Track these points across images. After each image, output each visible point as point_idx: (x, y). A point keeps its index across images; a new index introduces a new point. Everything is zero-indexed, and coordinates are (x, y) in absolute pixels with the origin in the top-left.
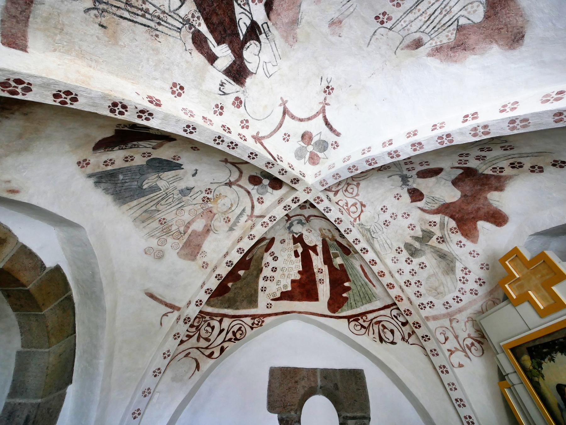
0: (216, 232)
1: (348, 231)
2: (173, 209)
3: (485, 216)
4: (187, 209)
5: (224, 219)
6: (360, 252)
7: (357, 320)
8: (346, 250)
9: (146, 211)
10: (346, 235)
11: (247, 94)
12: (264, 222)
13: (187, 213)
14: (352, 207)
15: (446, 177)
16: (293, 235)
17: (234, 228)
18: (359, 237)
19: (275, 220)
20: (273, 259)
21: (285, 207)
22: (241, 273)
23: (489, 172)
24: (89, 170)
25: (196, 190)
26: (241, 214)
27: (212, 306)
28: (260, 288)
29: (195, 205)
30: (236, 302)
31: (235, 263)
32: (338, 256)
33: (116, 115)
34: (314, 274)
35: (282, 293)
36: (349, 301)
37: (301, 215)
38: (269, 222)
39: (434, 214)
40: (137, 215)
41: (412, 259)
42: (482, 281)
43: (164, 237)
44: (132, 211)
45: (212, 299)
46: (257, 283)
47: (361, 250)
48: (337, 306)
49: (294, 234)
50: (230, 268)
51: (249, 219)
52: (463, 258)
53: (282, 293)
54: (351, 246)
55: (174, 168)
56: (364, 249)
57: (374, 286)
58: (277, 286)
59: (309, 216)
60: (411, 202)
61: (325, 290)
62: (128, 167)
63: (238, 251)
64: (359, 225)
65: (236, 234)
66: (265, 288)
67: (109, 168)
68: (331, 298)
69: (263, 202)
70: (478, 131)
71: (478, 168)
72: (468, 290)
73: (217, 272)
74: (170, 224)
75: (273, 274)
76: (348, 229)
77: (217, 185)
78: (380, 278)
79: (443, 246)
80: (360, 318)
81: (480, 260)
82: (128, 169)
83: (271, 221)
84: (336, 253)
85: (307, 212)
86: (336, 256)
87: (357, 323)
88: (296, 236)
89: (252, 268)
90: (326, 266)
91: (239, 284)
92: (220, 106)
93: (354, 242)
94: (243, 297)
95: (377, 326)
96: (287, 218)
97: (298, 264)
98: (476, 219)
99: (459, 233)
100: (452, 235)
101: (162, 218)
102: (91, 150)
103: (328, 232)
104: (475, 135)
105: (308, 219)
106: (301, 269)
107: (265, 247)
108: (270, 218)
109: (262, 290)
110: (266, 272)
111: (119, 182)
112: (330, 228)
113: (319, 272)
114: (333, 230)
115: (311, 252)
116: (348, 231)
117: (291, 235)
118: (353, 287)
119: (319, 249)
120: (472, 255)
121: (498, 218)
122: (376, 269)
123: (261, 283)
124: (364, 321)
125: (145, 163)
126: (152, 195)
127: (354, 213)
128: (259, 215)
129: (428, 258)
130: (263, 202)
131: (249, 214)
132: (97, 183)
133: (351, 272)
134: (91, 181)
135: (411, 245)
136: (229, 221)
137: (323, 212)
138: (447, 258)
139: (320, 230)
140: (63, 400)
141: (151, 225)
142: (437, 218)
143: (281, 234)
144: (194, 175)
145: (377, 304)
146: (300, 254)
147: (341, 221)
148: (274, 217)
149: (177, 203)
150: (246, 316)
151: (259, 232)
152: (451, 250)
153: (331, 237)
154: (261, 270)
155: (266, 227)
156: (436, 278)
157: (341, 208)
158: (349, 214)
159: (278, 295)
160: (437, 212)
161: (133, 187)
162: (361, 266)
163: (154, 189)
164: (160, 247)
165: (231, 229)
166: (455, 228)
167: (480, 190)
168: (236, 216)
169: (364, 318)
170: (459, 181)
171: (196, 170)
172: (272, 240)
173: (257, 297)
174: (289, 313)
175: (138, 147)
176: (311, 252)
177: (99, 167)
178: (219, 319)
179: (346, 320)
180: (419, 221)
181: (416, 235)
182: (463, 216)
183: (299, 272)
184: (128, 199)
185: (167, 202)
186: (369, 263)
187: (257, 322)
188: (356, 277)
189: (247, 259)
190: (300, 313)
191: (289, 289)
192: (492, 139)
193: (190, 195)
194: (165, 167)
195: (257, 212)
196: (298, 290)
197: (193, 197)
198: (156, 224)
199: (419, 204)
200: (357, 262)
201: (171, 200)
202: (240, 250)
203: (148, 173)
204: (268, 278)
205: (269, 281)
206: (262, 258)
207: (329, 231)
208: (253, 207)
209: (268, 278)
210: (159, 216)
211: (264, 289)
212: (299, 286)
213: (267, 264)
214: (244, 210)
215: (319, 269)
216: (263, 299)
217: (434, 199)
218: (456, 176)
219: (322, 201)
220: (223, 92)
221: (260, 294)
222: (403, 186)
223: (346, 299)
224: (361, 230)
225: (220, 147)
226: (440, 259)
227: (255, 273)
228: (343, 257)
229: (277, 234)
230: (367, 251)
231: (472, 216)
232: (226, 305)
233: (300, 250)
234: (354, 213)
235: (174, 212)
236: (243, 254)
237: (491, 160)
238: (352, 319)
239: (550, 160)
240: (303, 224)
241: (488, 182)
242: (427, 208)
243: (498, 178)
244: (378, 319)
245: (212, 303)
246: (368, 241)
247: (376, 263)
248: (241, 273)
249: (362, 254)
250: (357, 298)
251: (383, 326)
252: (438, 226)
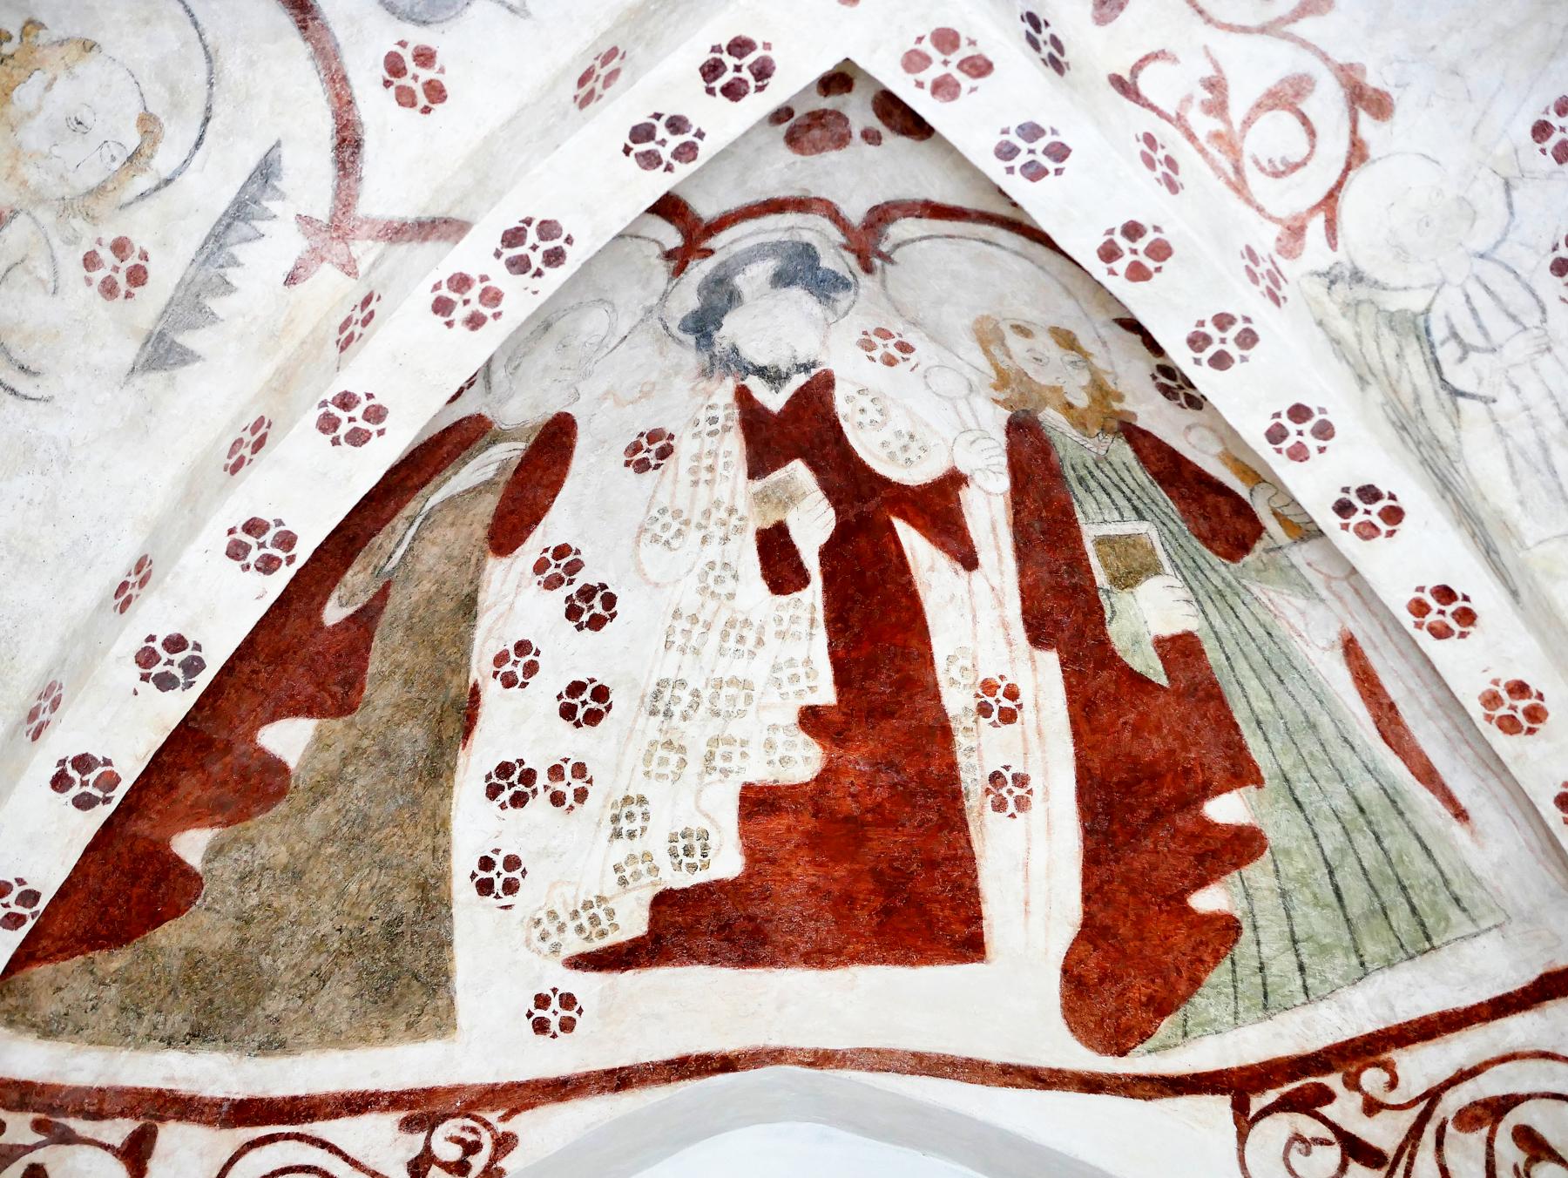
0: (23, 384)
1: (1227, 340)
5: (90, 261)
6: (1328, 521)
7: (1310, 1102)
8: (1222, 516)
10: (1203, 378)
12: (461, 282)
14: (1266, 120)
16: (743, 395)
17: (187, 340)
18: (1329, 391)
19: (555, 258)
20: (572, 613)
21: (642, 133)
22: (288, 739)
26: (241, 211)
27: (47, 1031)
28: (463, 865)
30: (254, 987)
31: (216, 657)
32: (1154, 569)
34: (944, 732)
35: (664, 901)
36: (1245, 947)
37: (801, 205)
38: (501, 277)
45: (41, 973)
46: (440, 826)
47: (1344, 508)
48: (1140, 988)
49: (756, 385)
50: (179, 703)
51: (316, 256)
53: (664, 901)
54: (1255, 475)
56: (1369, 494)
57: (1461, 814)
58: (622, 849)
59: (881, 216)
61: (1037, 866)
63: (236, 551)
64: (1331, 279)
65: (213, 396)
66: (512, 863)
68: (1091, 932)
69: (436, 92)
73: (63, 742)
75: (573, 742)
76: (1223, 321)
78: (1503, 744)
80: (1333, 1081)
83: (520, 265)
84: (1130, 542)
85: (861, 175)
86: (1134, 567)
87: (1309, 1127)
88: (774, 400)
89: (383, 692)
90: (1050, 660)
91: (272, 837)
93: (1276, 435)
94: (320, 943)
95: (1477, 1138)
96: (672, 237)
97: (793, 653)
103: (1054, 352)
105: (867, 240)
106: (825, 694)
107: (488, 505)
108: (513, 237)
109: (485, 887)
110: (515, 726)
112: (1068, 314)
113: (984, 710)
114: (1094, 332)
115: (910, 538)
116: (1227, 340)
117: (724, 394)
118: (1279, 827)
119: (987, 510)
122: (1469, 666)
123: (475, 825)
124: (1372, 1107)
127: (1283, 170)
128: (407, 210)
130: (436, 92)
131: (322, 209)
133: (1262, 705)
136: (137, 276)
137: (995, 170)
139: (988, 336)
143: (627, 378)
145: (1497, 967)
146: (812, 562)
147: (1161, 251)
148: (548, 229)
150: (356, 1104)
151: (415, 376)
153: (1081, 401)
154: (468, 712)
155: (475, 322)
157: (1167, 133)
158: (1239, 187)
159: (633, 922)
162: (1350, 648)
165: (162, 353)
168: (200, 227)
169: (1372, 1079)
172: (554, 443)
173: (444, 944)
174: (727, 1064)
176: (910, 538)
178: (118, 1131)
179: (1219, 1107)
183: (811, 719)
186: (1408, 620)
187: (453, 1153)
188: (1309, 745)
189: (333, 613)
190: (822, 1059)
191: (727, 863)
192: (228, 669)
195: (387, 190)
196: (804, 873)
200: (1317, 612)
202: (252, 541)
204: (528, 777)
205: (539, 805)
206: (468, 607)
207: (1067, 340)
208: (348, 143)
209: (528, 777)
211: (498, 878)
212: (814, 842)
213: (520, 662)
214: (266, 172)
215: (988, 687)
216: (495, 965)
219: (979, 67)
221: (470, 915)
223: (1226, 929)
224: (1343, 327)
227: (413, 737)
228: (1191, 576)
229: (591, 389)
230: (1394, 515)
232: (177, 1021)
233: (813, 526)
234: (1283, 170)
236: (285, 575)
238: (1271, 1096)
240: (825, 286)
244: (1490, 1086)
245: (50, 1006)
246: (1406, 424)
247: (1467, 617)
248: (288, 739)
249: (1347, 542)
250: (1316, 921)
251: (1527, 1137)
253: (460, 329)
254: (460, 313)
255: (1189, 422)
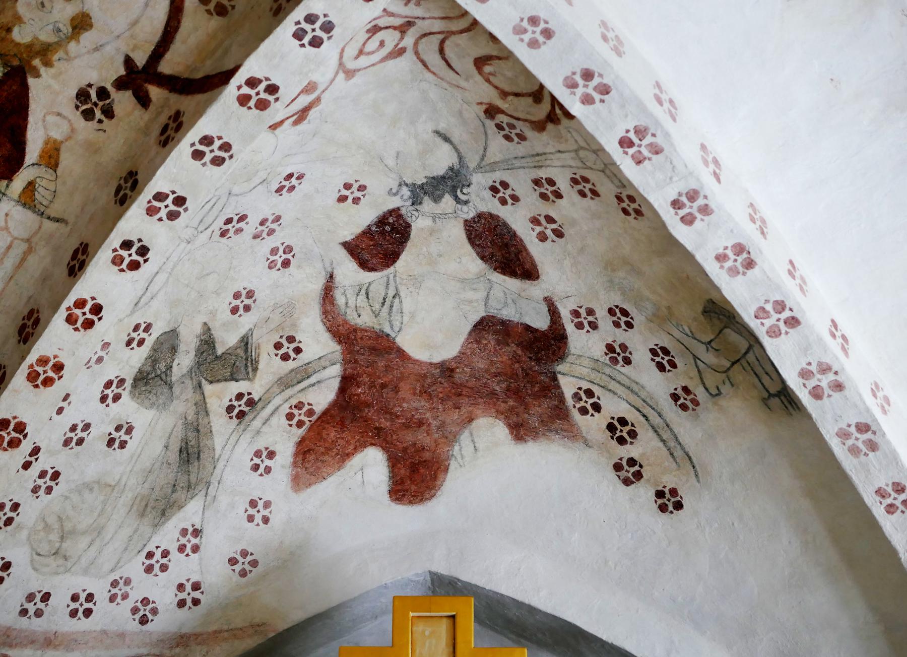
3: (405, 450)
15: (497, 292)
23: (568, 386)
39: (329, 330)
41: (125, 396)
42: (196, 594)
52: (223, 500)
60: (346, 245)
70: (819, 376)
71: (570, 359)
72: (136, 596)
79: (221, 426)
81: (255, 538)
98: (379, 437)
99: (301, 432)
100: (280, 420)
104: (805, 374)
120: (251, 511)
121: (415, 478)
129: (153, 426)
135: (174, 350)
138: (193, 468)
140: (201, 116)
142: (318, 343)
152: (225, 457)
156: (104, 503)
160: (344, 334)
166: (310, 413)
167: (493, 393)
170: (496, 332)
180: (275, 307)
181: (217, 334)
182: (368, 405)
199: (349, 272)
217: (390, 301)
218: (515, 318)
222: (406, 192)
226: (173, 456)
231: (385, 424)
237: (619, 377)
239: (669, 481)
241: (529, 399)
242: (340, 300)
243: (560, 413)
252: (291, 365)
255: (65, 113)
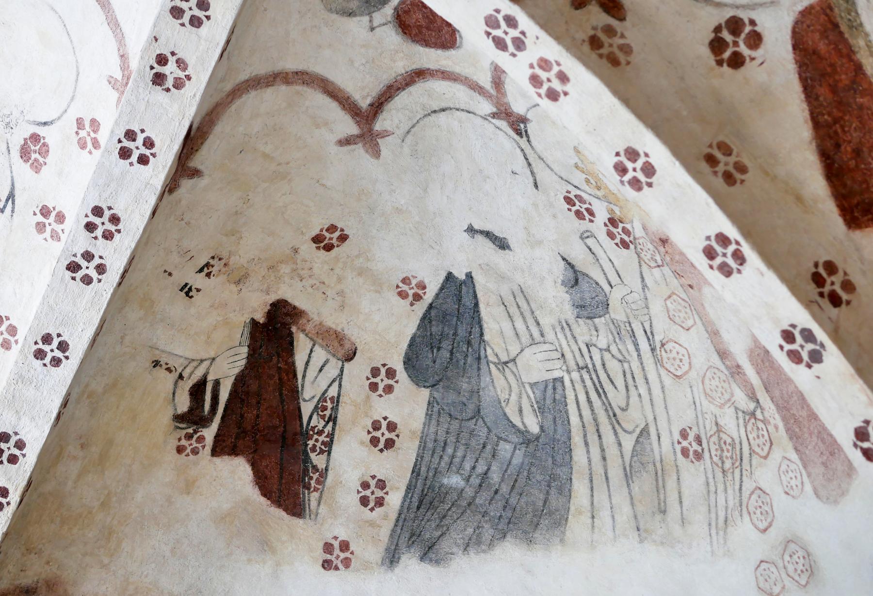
2: (652, 376)
4: (662, 328)
9: (628, 476)
11: (16, 114)
13: (683, 338)
24: (368, 550)
25: (578, 255)
29: (644, 286)
33: (8, 503)
40: (627, 509)
43: (748, 486)
44: (605, 515)
55: (467, 301)
62: (423, 446)
67: (395, 499)
74: (711, 429)
77: (538, 166)
82: (430, 448)
92: (40, 218)
101: (677, 436)
102: (300, 522)
111: (469, 492)
125: (425, 394)
126: (574, 419)
132: (429, 552)
134: (411, 565)
141: (686, 493)
144: (502, 244)
149: (631, 347)
161: (517, 460)
163: (550, 398)
164: (772, 531)
171: (471, 230)
175: (336, 401)
177: (372, 524)
184: (555, 501)
185: (620, 382)
193: (606, 288)
194: (462, 332)
197: (614, 279)
198: (693, 477)
201: (614, 366)
203: (475, 393)
210: (665, 446)
220: (7, 200)
225: (116, 265)
235: (668, 380)
236: (747, 250)
253: (568, 88)
254: (556, 85)
